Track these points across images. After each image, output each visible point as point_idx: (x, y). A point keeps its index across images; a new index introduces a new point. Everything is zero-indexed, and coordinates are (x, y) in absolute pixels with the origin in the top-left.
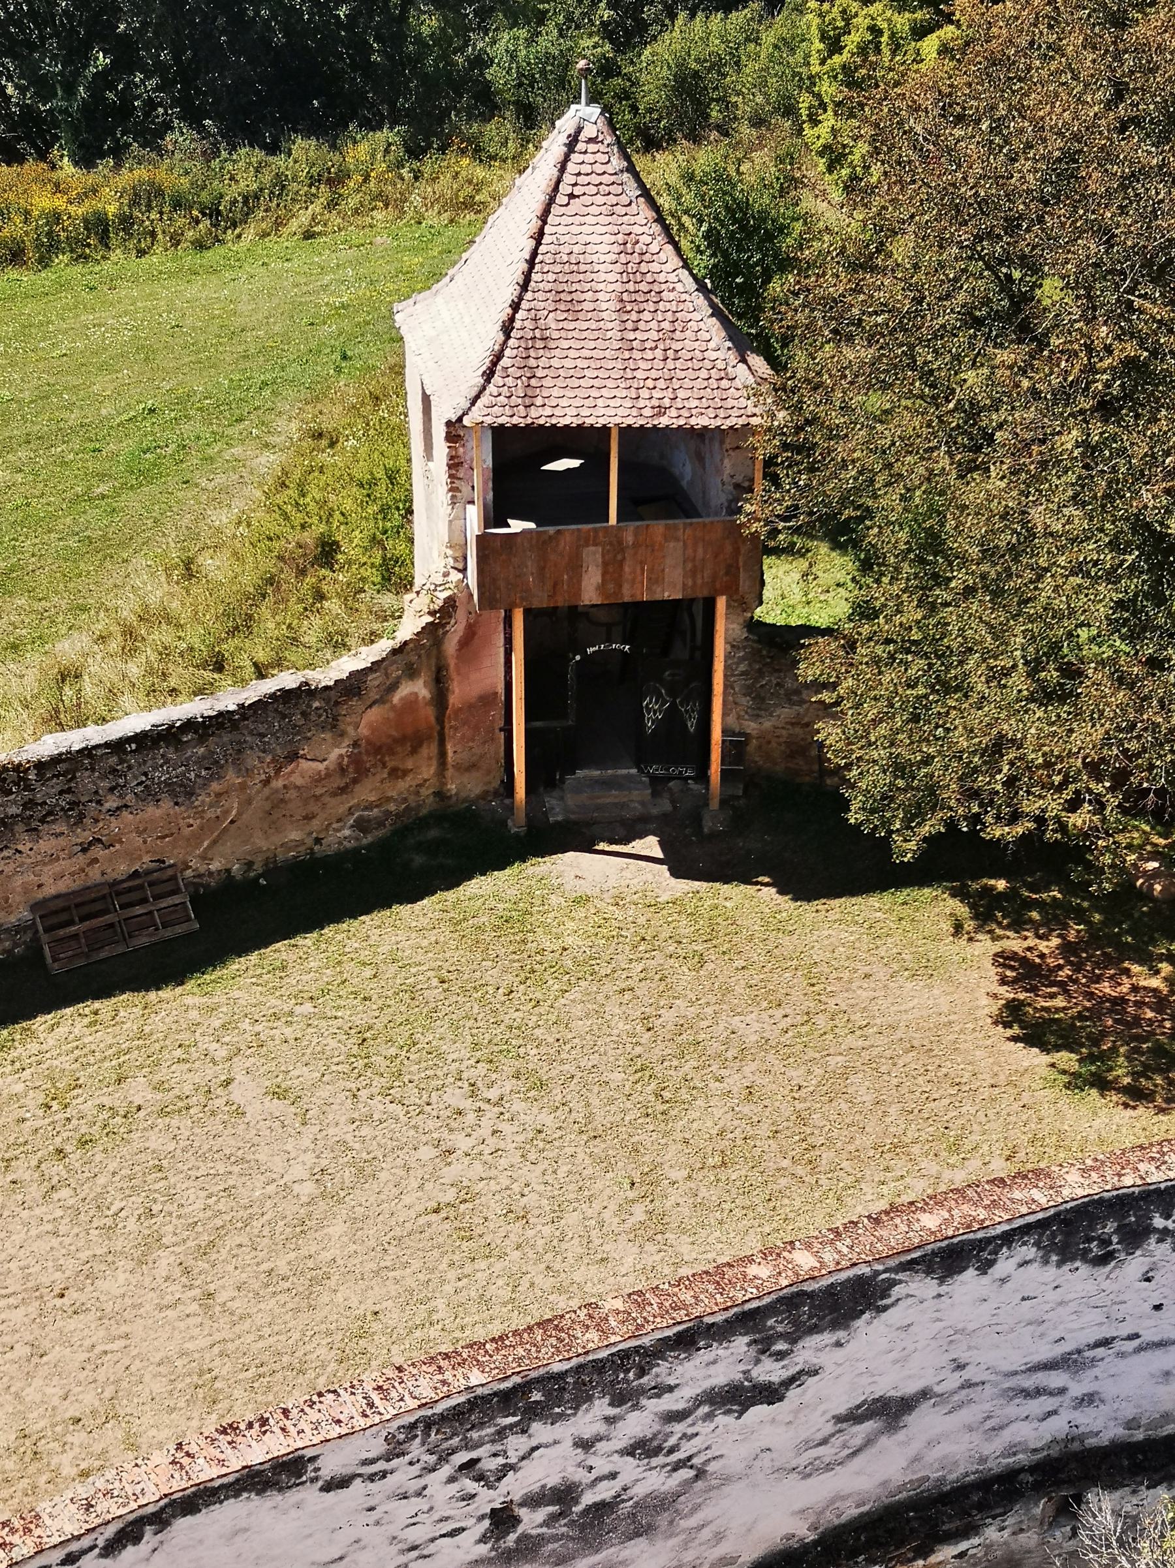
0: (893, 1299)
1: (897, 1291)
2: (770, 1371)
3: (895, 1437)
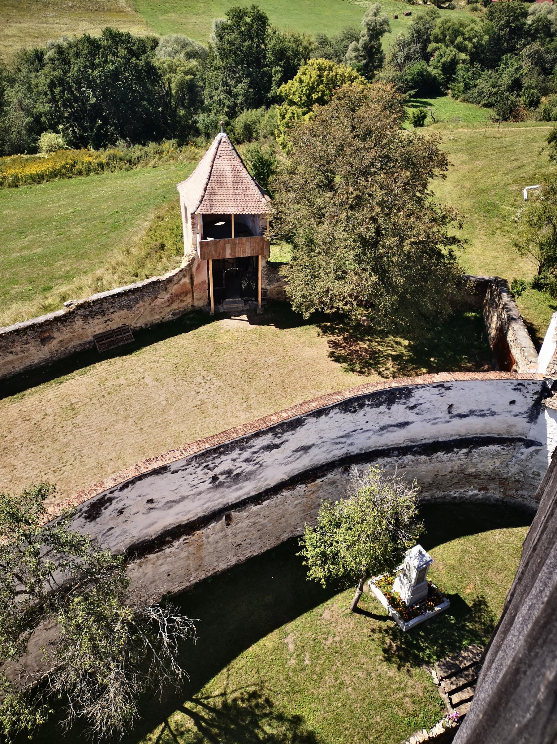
2: (277, 441)
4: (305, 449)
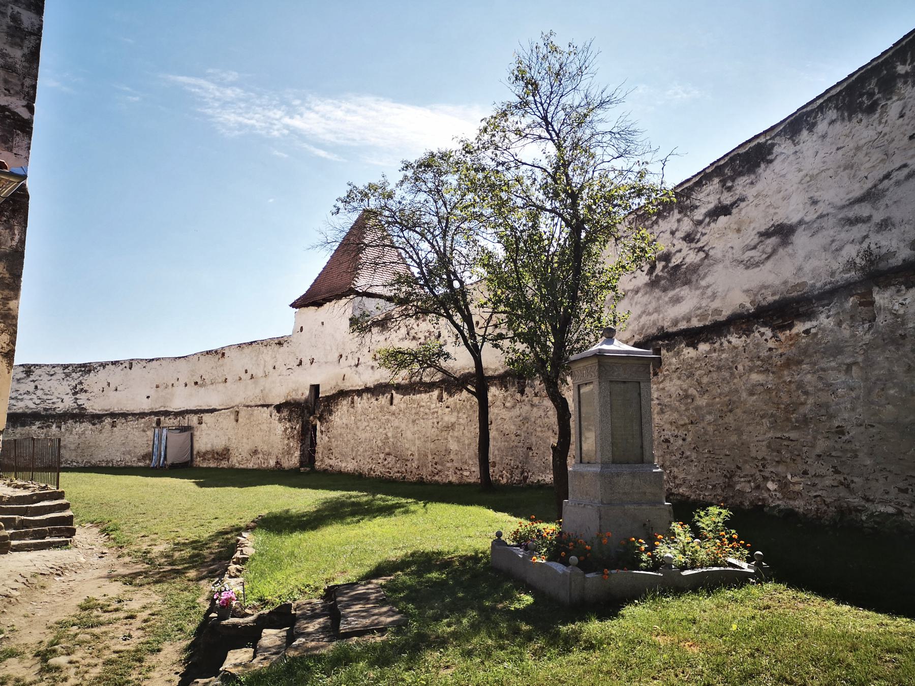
0: (774, 155)
1: (776, 150)
2: (727, 199)
3: (786, 249)
4: (783, 233)
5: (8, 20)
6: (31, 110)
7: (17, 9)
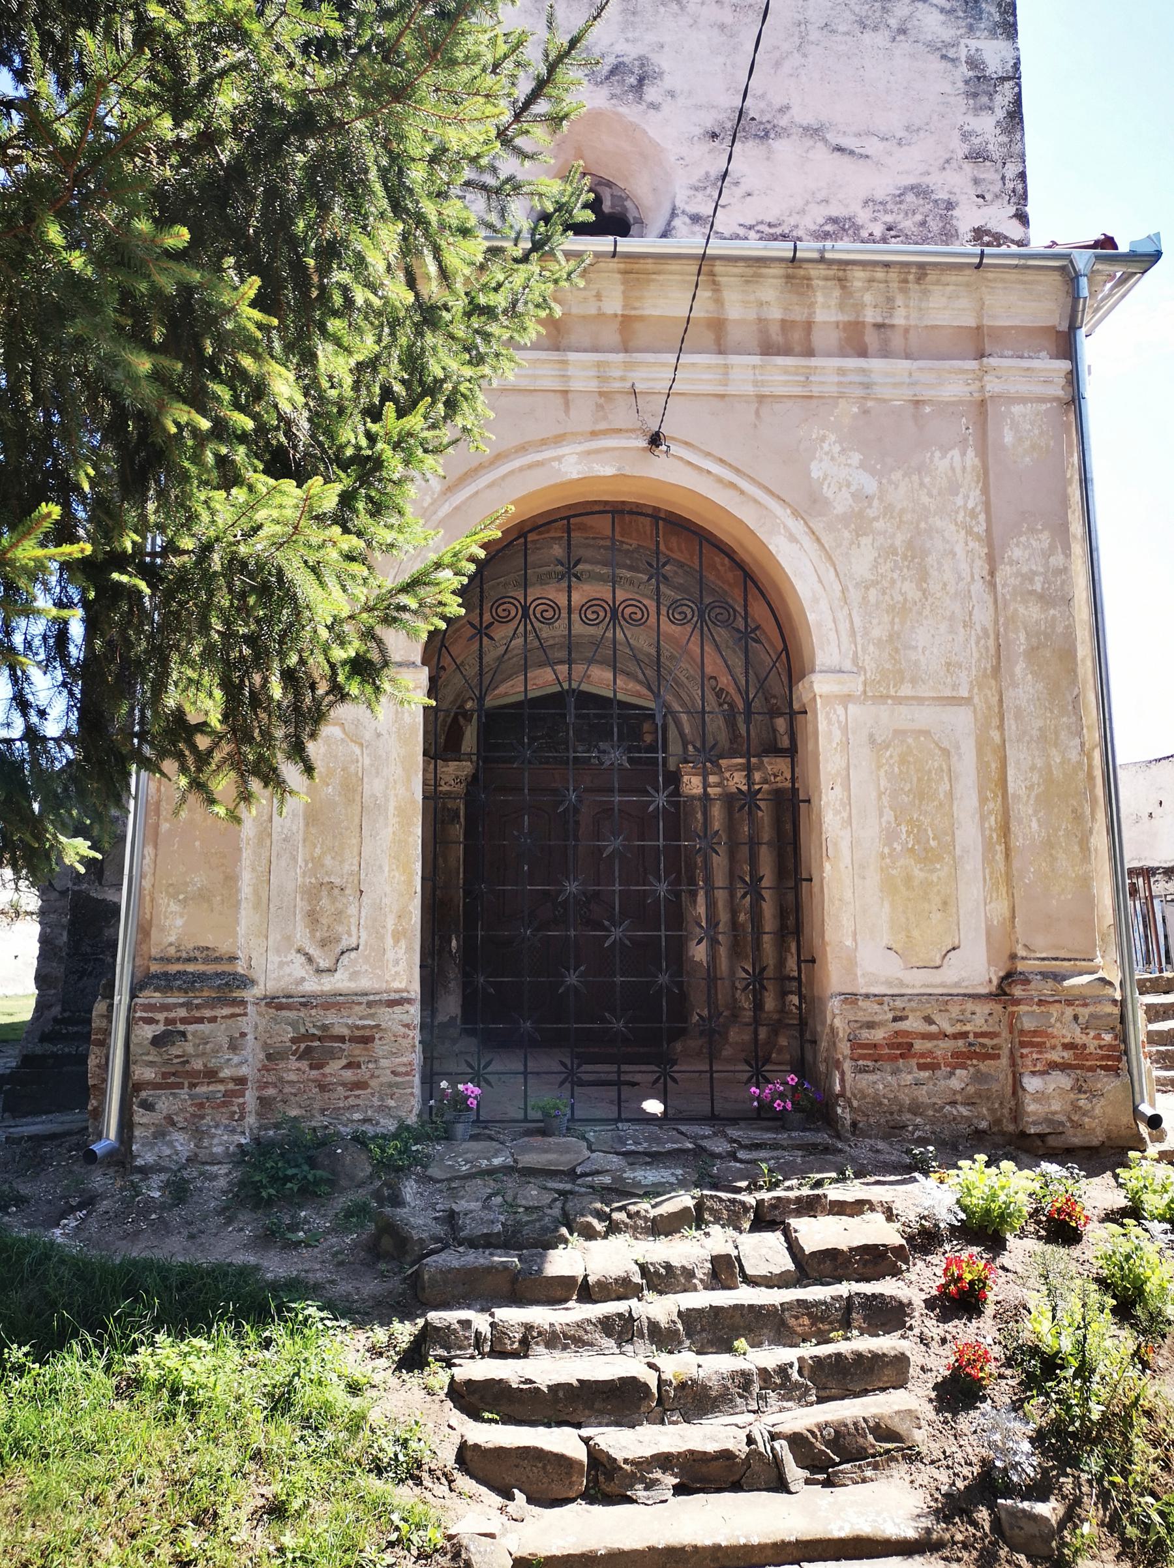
5: (964, 68)
6: (1023, 218)
7: (974, 44)
